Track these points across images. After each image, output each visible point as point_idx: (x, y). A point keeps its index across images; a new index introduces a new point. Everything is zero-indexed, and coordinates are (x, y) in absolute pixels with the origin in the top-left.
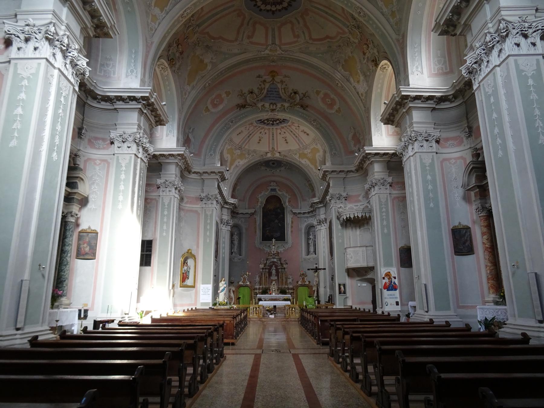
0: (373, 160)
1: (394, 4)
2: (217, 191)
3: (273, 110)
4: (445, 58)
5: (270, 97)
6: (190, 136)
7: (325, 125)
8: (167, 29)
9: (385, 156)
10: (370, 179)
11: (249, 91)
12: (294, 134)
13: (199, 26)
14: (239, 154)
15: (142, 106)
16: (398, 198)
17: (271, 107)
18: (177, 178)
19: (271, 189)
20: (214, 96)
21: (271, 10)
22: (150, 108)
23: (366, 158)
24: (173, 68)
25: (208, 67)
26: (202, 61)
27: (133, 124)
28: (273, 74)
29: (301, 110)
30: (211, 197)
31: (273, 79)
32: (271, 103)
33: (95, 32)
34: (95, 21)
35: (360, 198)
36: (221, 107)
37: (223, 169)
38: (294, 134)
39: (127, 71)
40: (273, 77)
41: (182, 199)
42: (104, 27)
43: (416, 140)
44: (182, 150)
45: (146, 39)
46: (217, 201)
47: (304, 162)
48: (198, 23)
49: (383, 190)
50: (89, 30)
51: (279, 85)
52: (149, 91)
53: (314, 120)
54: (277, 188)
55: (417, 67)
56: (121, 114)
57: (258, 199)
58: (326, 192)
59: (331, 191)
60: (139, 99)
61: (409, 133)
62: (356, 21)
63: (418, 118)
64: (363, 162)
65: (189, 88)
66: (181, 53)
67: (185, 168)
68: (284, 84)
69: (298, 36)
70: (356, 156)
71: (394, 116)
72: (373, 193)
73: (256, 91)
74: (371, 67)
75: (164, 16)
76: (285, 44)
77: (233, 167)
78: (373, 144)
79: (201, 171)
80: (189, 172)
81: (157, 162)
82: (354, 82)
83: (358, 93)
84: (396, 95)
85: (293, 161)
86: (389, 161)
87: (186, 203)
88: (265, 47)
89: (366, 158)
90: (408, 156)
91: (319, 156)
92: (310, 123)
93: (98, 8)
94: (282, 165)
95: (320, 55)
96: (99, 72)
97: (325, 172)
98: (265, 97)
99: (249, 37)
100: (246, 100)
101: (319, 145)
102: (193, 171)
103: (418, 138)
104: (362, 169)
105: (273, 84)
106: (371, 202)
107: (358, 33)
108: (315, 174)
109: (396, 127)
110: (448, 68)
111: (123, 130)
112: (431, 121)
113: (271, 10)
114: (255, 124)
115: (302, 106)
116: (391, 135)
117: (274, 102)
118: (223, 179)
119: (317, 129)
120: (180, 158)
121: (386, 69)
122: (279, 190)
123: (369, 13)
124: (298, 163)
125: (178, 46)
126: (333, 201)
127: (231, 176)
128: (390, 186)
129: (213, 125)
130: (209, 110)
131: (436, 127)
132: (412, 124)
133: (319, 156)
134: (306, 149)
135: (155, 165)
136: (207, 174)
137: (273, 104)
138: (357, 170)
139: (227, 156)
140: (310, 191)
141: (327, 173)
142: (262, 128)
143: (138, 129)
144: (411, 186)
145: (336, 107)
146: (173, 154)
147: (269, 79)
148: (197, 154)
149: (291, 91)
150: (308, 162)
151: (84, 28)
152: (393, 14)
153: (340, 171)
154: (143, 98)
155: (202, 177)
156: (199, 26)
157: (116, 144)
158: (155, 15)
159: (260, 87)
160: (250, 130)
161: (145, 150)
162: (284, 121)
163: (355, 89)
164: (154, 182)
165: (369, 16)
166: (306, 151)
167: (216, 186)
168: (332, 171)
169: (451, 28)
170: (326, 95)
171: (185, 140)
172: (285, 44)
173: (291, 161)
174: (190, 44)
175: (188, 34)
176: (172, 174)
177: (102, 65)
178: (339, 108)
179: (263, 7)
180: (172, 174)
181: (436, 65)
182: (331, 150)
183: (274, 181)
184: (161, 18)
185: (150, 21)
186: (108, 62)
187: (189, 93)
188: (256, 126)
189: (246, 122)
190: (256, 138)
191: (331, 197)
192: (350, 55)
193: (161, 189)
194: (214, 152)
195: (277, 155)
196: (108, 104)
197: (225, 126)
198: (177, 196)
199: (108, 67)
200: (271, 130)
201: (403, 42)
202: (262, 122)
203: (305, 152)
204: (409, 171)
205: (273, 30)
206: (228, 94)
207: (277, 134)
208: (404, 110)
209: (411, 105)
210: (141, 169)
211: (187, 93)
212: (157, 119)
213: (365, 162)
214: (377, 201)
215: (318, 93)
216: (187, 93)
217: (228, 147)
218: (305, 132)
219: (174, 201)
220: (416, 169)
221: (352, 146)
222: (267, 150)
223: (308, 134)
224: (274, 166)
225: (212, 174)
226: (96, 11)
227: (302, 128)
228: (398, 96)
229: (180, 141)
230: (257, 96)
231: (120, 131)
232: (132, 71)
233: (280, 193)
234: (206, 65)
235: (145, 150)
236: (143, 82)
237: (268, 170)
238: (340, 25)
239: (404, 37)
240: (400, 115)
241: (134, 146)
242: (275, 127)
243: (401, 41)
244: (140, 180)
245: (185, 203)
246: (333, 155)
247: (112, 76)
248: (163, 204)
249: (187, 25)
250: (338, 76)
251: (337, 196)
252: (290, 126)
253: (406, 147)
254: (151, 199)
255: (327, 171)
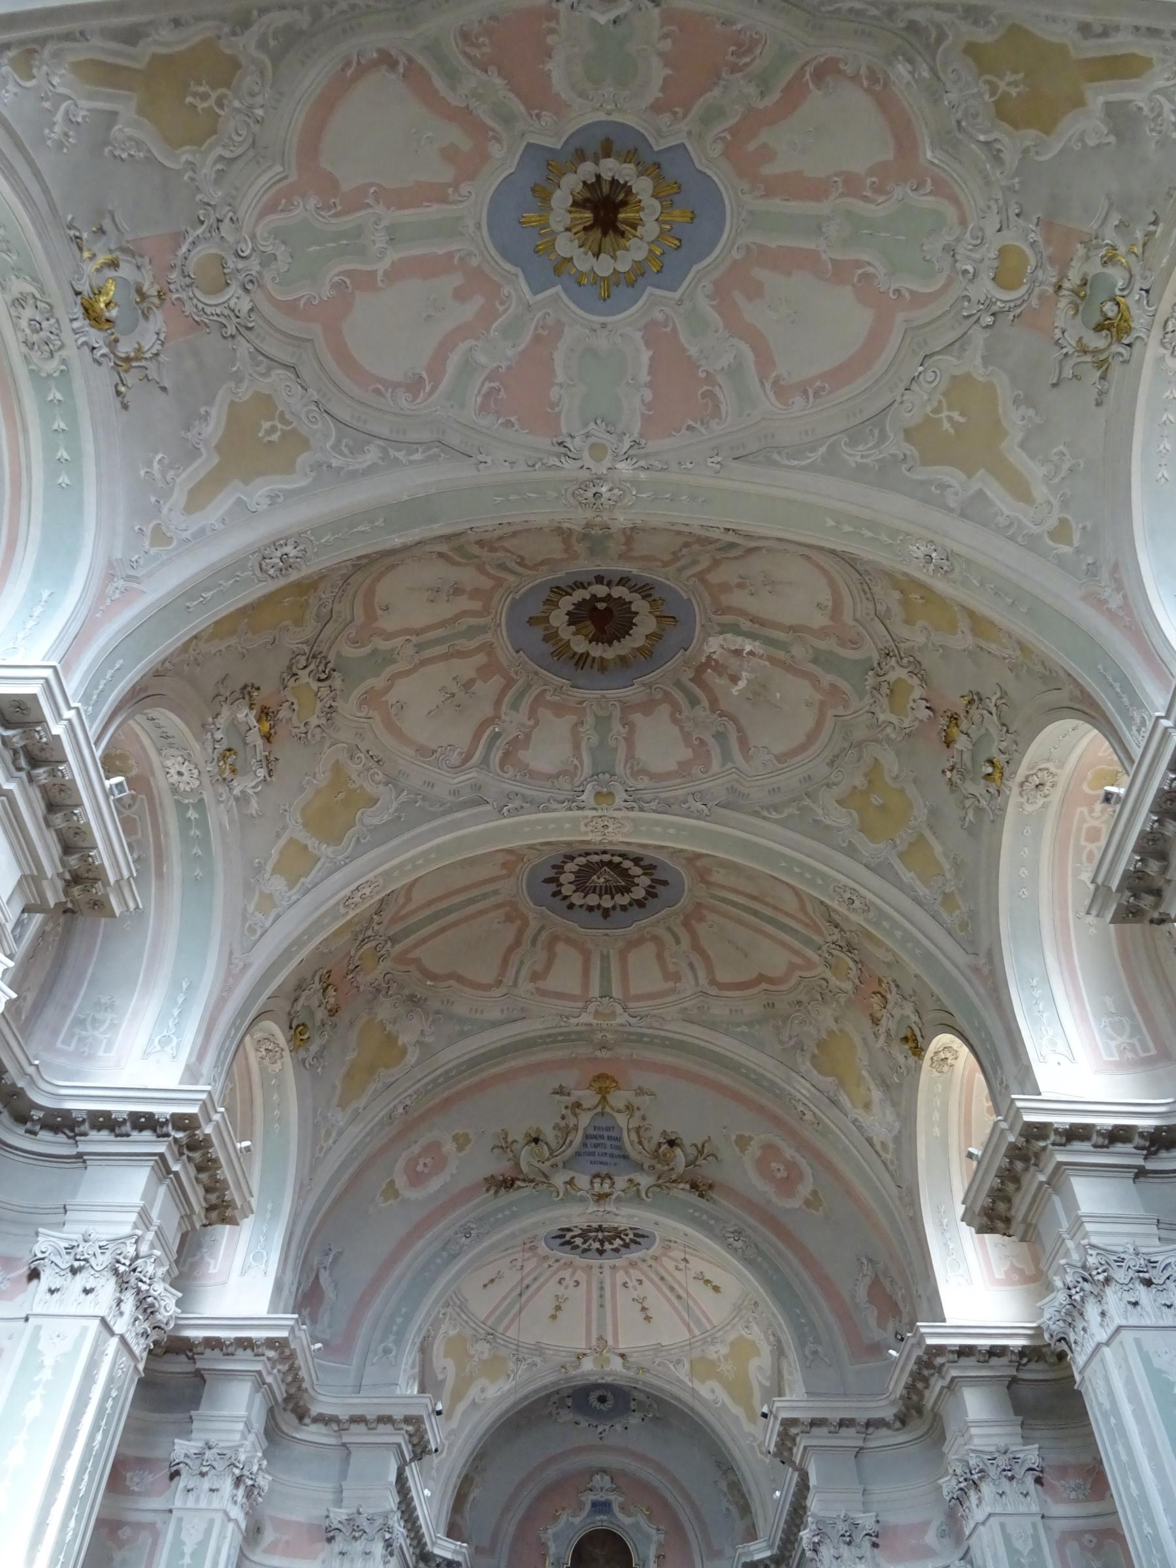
0: (954, 1373)
1: (948, 876)
2: (392, 1501)
3: (601, 1197)
4: (1132, 1016)
5: (593, 1154)
6: (324, 1277)
7: (772, 1247)
8: (295, 935)
9: (994, 1361)
10: (954, 1452)
11: (527, 1135)
12: (672, 1289)
13: (394, 940)
14: (486, 1356)
15: (169, 1146)
16: (1077, 1535)
17: (597, 1186)
18: (251, 1437)
19: (595, 1504)
20: (416, 1149)
21: (599, 906)
22: (197, 1155)
23: (929, 1365)
24: (302, 1054)
25: (408, 1057)
26: (391, 1039)
27: (123, 1208)
28: (603, 1083)
29: (693, 1198)
30: (365, 1525)
31: (604, 1099)
32: (597, 1176)
33: (66, 893)
34: (73, 861)
35: (931, 1538)
36: (435, 1184)
37: (421, 1406)
38: (672, 1289)
39: (151, 1041)
40: (603, 1093)
41: (253, 1532)
42: (96, 880)
43: (1107, 1280)
44: (283, 1325)
45: (231, 954)
46: (388, 1544)
47: (709, 1394)
48: (391, 933)
49: (1013, 1503)
50: (45, 883)
51: (622, 1120)
52: (204, 1096)
53: (739, 1233)
54: (616, 1499)
55: (1053, 1043)
56: (95, 1171)
57: (544, 1545)
58: (797, 1513)
59: (814, 1504)
60: (163, 1124)
61: (1075, 1257)
62: (842, 930)
63: (1096, 1204)
64: (920, 1385)
65: (340, 1118)
66: (333, 1012)
67: (287, 1400)
68: (637, 1114)
69: (676, 977)
70: (895, 1362)
71: (1008, 1200)
72: (979, 1515)
73: (549, 1135)
74: (901, 1059)
75: (294, 898)
76: (639, 998)
77: (462, 1407)
78: (948, 1311)
79: (344, 1414)
80: (301, 1415)
81: (190, 1368)
82: (854, 1107)
83: (869, 1141)
84: (1004, 1125)
85: (667, 1387)
86: (1014, 1380)
87: (271, 1550)
88: (580, 1005)
89: (929, 1365)
90: (1089, 1349)
91: (760, 1368)
92: (722, 1240)
93: (88, 824)
94: (633, 1405)
95: (744, 1029)
96: (63, 1042)
97: (789, 1423)
98: (578, 1154)
99: (535, 977)
100: (517, 1165)
101: (756, 1328)
102: (315, 1410)
103: (1111, 1272)
104: (919, 1412)
105: (603, 1114)
106: (976, 1552)
107: (851, 964)
108: (751, 1440)
109: (1023, 1240)
110: (1151, 1044)
111: (82, 1228)
112: (1142, 1213)
113: (599, 906)
114: (543, 1249)
115: (694, 1186)
116: (1001, 1283)
117: (604, 1170)
118: (421, 1450)
119: (749, 1262)
120: (271, 1354)
121: (952, 1056)
122: (622, 1508)
123: (878, 902)
124: (687, 1397)
125: (325, 990)
126: (826, 1552)
127: (453, 1439)
128: (1038, 1481)
129: (405, 1243)
130: (396, 1194)
131: (1164, 1234)
132: (1077, 1223)
133: (759, 1367)
134: (713, 1343)
135: (172, 1375)
136: (362, 1428)
137: (602, 1177)
138: (903, 1420)
139: (444, 1366)
140: (734, 1511)
141: (793, 1431)
142: (570, 1264)
143: (135, 1226)
144: (1132, 1466)
145: (805, 1189)
146: (249, 1340)
147: (589, 1098)
148: (336, 1348)
149: (657, 1138)
150: (723, 1396)
151: (33, 877)
152: (947, 898)
153: (843, 1423)
154: (179, 1121)
155: (346, 1439)
156: (394, 940)
157: (48, 1278)
158: (271, 895)
159: (563, 1124)
160: (526, 1270)
161: (146, 1306)
162: (639, 1238)
163: (860, 1128)
164: (160, 1453)
165: (878, 909)
166: (712, 1349)
167: (392, 1477)
168: (814, 1423)
169: (1147, 901)
170: (768, 1148)
171: (306, 1293)
172: (639, 998)
173: (661, 1389)
174: (362, 988)
175: (360, 959)
176: (234, 1419)
177: (80, 1022)
178: (815, 1193)
179: (577, 899)
180: (234, 1419)
181: (1113, 1039)
182: (801, 1343)
183: (604, 1471)
184: (285, 903)
185: (251, 908)
186: (99, 1016)
187: (341, 1132)
188: (546, 1258)
189: (513, 1236)
190: (543, 1302)
191: (819, 1532)
192: (834, 1027)
193: (182, 1482)
194: (399, 1342)
195: (616, 1365)
196: (61, 1138)
197: (444, 1248)
198: (237, 1513)
199: (94, 1028)
200: (596, 1271)
201: (992, 972)
202: (564, 1239)
203: (712, 1353)
204: (1107, 1405)
205: (605, 958)
206: (461, 1141)
207: (614, 1286)
208: (1042, 1178)
209: (1061, 1158)
210: (111, 1380)
211: (334, 1134)
212: (213, 1198)
213: (926, 1380)
214: (1002, 1551)
215: (742, 1142)
216: (334, 1134)
217: (448, 1330)
218: (707, 1282)
219: (221, 1536)
220: (1134, 1397)
221: (873, 1323)
222: (581, 1345)
223: (716, 1289)
224: (604, 1407)
225: (382, 1428)
226: (82, 832)
227: (696, 1265)
228: (1011, 1129)
229: (285, 1292)
230: (552, 1152)
231: (72, 1233)
232: (165, 1042)
233: (626, 1520)
234: (404, 1051)
235: (146, 1306)
236: (191, 1073)
237: (584, 1424)
238: (796, 944)
239: (993, 958)
240: (1028, 1199)
241: (107, 1288)
242: (607, 1263)
243: (985, 971)
244: (95, 1428)
245: (266, 1551)
246: (810, 1362)
247: (101, 1053)
248: (178, 1543)
249: (361, 932)
250: (802, 1089)
251: (842, 1527)
252: (655, 1258)
253: (1074, 1311)
254: (138, 1526)
255: (793, 1422)
